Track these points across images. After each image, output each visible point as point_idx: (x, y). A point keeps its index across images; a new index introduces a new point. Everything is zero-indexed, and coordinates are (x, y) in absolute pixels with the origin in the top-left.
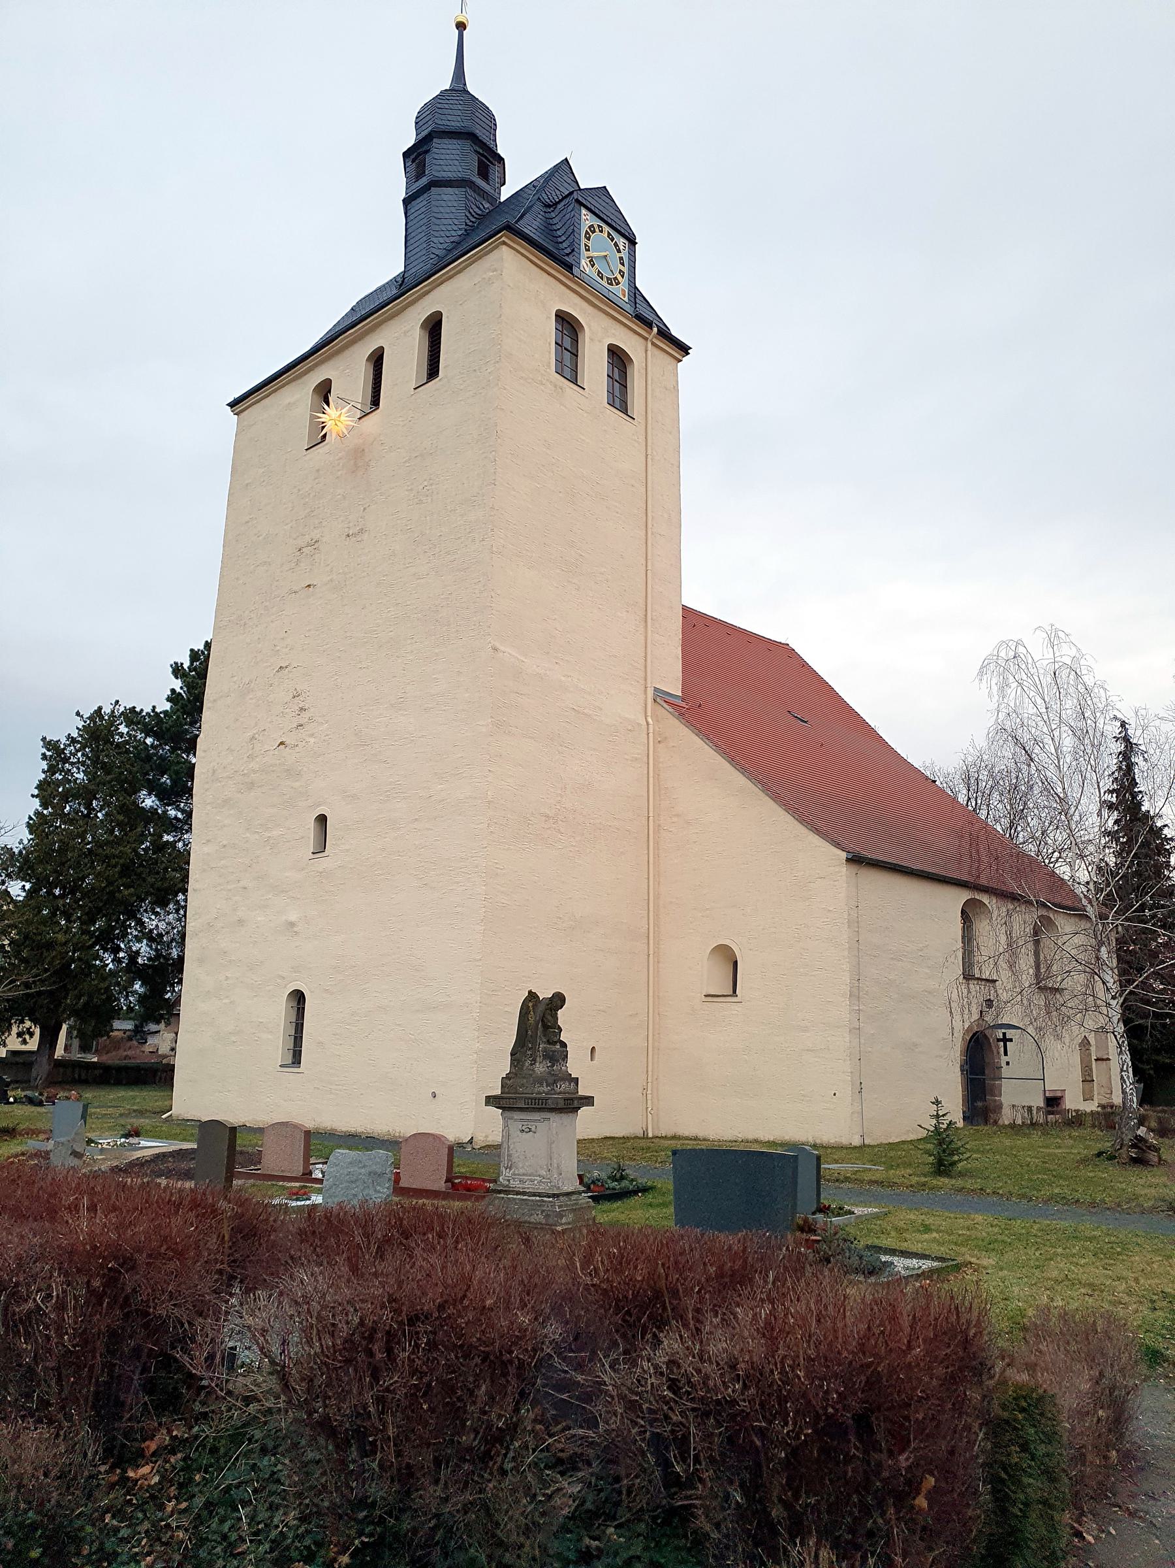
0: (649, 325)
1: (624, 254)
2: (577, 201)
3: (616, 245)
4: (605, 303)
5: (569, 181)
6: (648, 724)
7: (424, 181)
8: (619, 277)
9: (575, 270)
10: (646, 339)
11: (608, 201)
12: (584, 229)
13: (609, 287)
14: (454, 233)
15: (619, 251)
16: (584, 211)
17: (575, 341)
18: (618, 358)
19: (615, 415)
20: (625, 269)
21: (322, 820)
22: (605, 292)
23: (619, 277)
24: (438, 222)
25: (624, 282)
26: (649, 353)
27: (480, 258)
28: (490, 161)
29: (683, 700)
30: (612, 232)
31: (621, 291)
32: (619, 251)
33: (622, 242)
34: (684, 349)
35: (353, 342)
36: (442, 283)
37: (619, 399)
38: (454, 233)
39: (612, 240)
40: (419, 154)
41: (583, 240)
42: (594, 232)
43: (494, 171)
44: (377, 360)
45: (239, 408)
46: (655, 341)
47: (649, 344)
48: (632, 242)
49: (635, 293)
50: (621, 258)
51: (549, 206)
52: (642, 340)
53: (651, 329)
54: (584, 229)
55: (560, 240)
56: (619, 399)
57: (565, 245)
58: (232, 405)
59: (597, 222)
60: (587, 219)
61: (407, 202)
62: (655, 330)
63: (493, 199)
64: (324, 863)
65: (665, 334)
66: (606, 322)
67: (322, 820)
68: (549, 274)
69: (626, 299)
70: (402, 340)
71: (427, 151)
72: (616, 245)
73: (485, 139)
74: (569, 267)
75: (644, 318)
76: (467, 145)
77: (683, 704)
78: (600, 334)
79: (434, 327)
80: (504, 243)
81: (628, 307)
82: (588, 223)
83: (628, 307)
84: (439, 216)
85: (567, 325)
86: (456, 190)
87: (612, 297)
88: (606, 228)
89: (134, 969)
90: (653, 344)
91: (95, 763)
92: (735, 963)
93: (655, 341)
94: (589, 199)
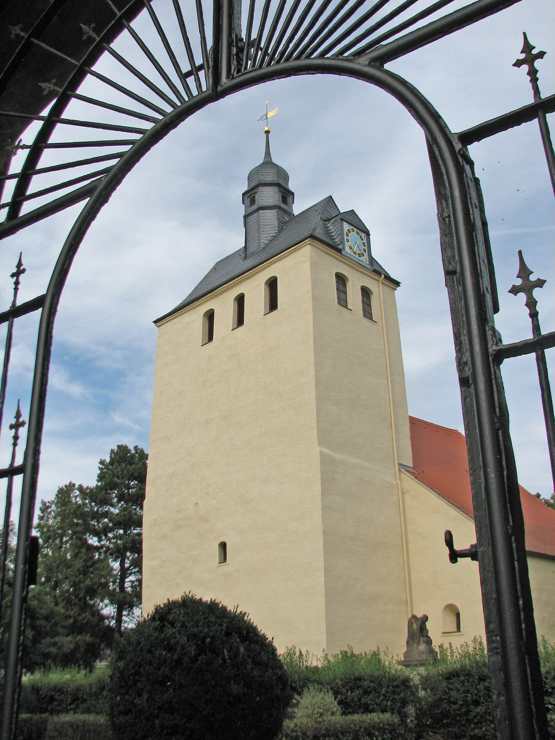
0: (379, 274)
1: (365, 241)
2: (341, 219)
3: (361, 237)
4: (358, 266)
5: (333, 206)
6: (398, 484)
7: (254, 207)
8: (364, 253)
9: (343, 252)
10: (378, 281)
11: (355, 216)
12: (345, 231)
13: (360, 258)
14: (272, 232)
15: (362, 240)
16: (344, 223)
17: (345, 286)
18: (366, 293)
19: (366, 321)
20: (366, 248)
21: (223, 546)
22: (358, 261)
23: (364, 253)
24: (264, 227)
25: (366, 254)
26: (381, 288)
27: (296, 251)
28: (287, 195)
29: (414, 468)
30: (358, 231)
31: (365, 259)
32: (362, 240)
33: (363, 235)
34: (397, 284)
35: (226, 291)
36: (276, 262)
37: (368, 313)
38: (272, 232)
39: (359, 234)
40: (251, 194)
41: (345, 237)
42: (350, 232)
43: (289, 199)
44: (240, 300)
45: (159, 324)
46: (384, 282)
47: (380, 284)
48: (368, 234)
49: (372, 260)
50: (364, 243)
51: (326, 221)
52: (376, 282)
53: (381, 276)
54: (345, 231)
55: (333, 238)
56: (368, 313)
57: (337, 240)
58: (155, 322)
59: (351, 227)
60: (346, 227)
61: (246, 217)
62: (383, 276)
63: (290, 214)
64: (225, 568)
65: (388, 278)
66: (358, 275)
67: (223, 546)
68: (330, 255)
69: (368, 263)
70: (254, 290)
71: (256, 193)
72: (361, 237)
73: (283, 185)
74: (340, 251)
75: (377, 271)
76: (276, 189)
77: (414, 471)
78: (356, 282)
79: (272, 284)
80: (309, 244)
81: (369, 267)
82: (347, 229)
83: (369, 267)
84: (264, 224)
85: (341, 279)
86: (272, 211)
87: (361, 263)
88: (355, 230)
89: (110, 543)
90: (382, 283)
91: (62, 515)
92: (458, 615)
93: (384, 282)
94: (347, 217)
